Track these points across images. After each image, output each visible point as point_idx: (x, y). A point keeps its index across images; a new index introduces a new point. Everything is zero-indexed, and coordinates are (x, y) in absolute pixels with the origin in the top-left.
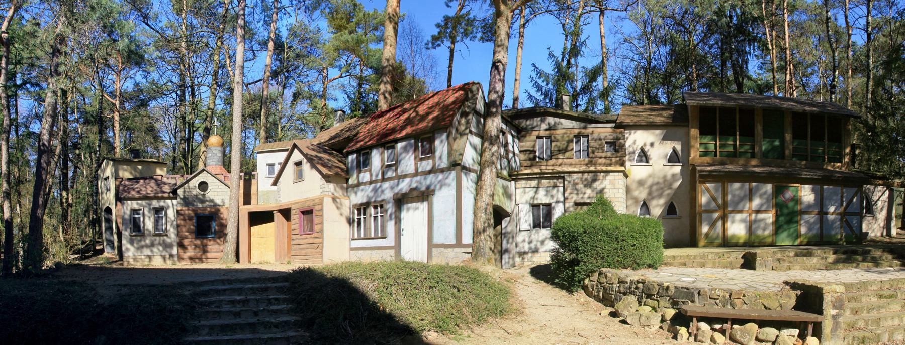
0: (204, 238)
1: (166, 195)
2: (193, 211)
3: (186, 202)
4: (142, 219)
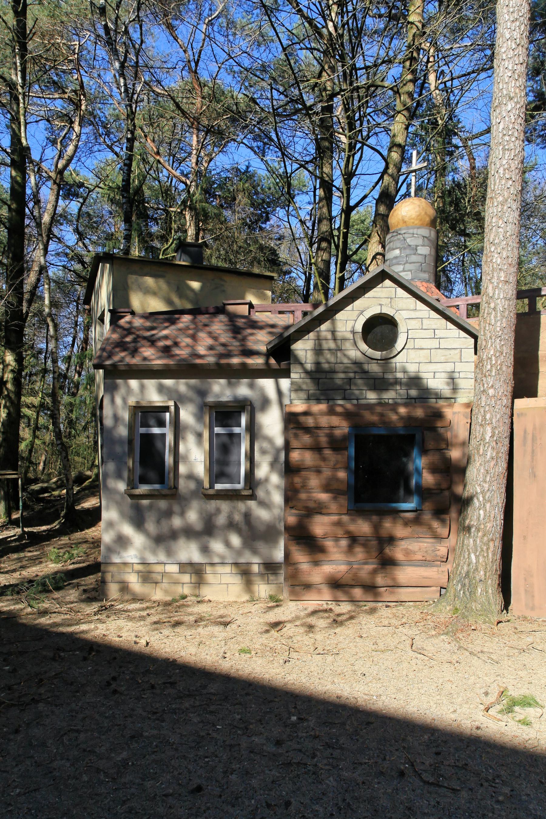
0: (383, 513)
1: (257, 361)
2: (347, 415)
3: (324, 382)
4: (170, 439)
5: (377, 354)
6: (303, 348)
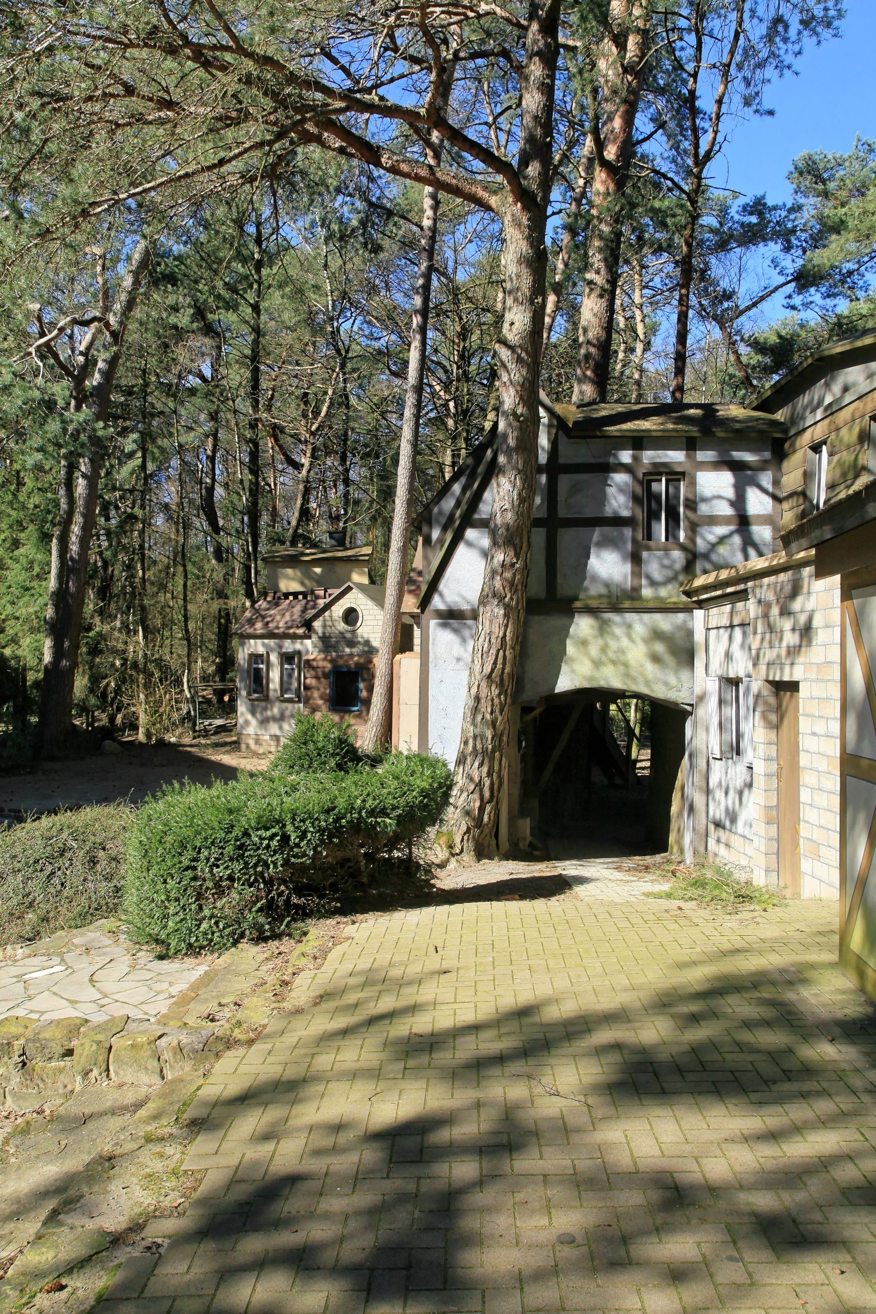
2: (332, 661)
5: (349, 628)
6: (317, 624)
